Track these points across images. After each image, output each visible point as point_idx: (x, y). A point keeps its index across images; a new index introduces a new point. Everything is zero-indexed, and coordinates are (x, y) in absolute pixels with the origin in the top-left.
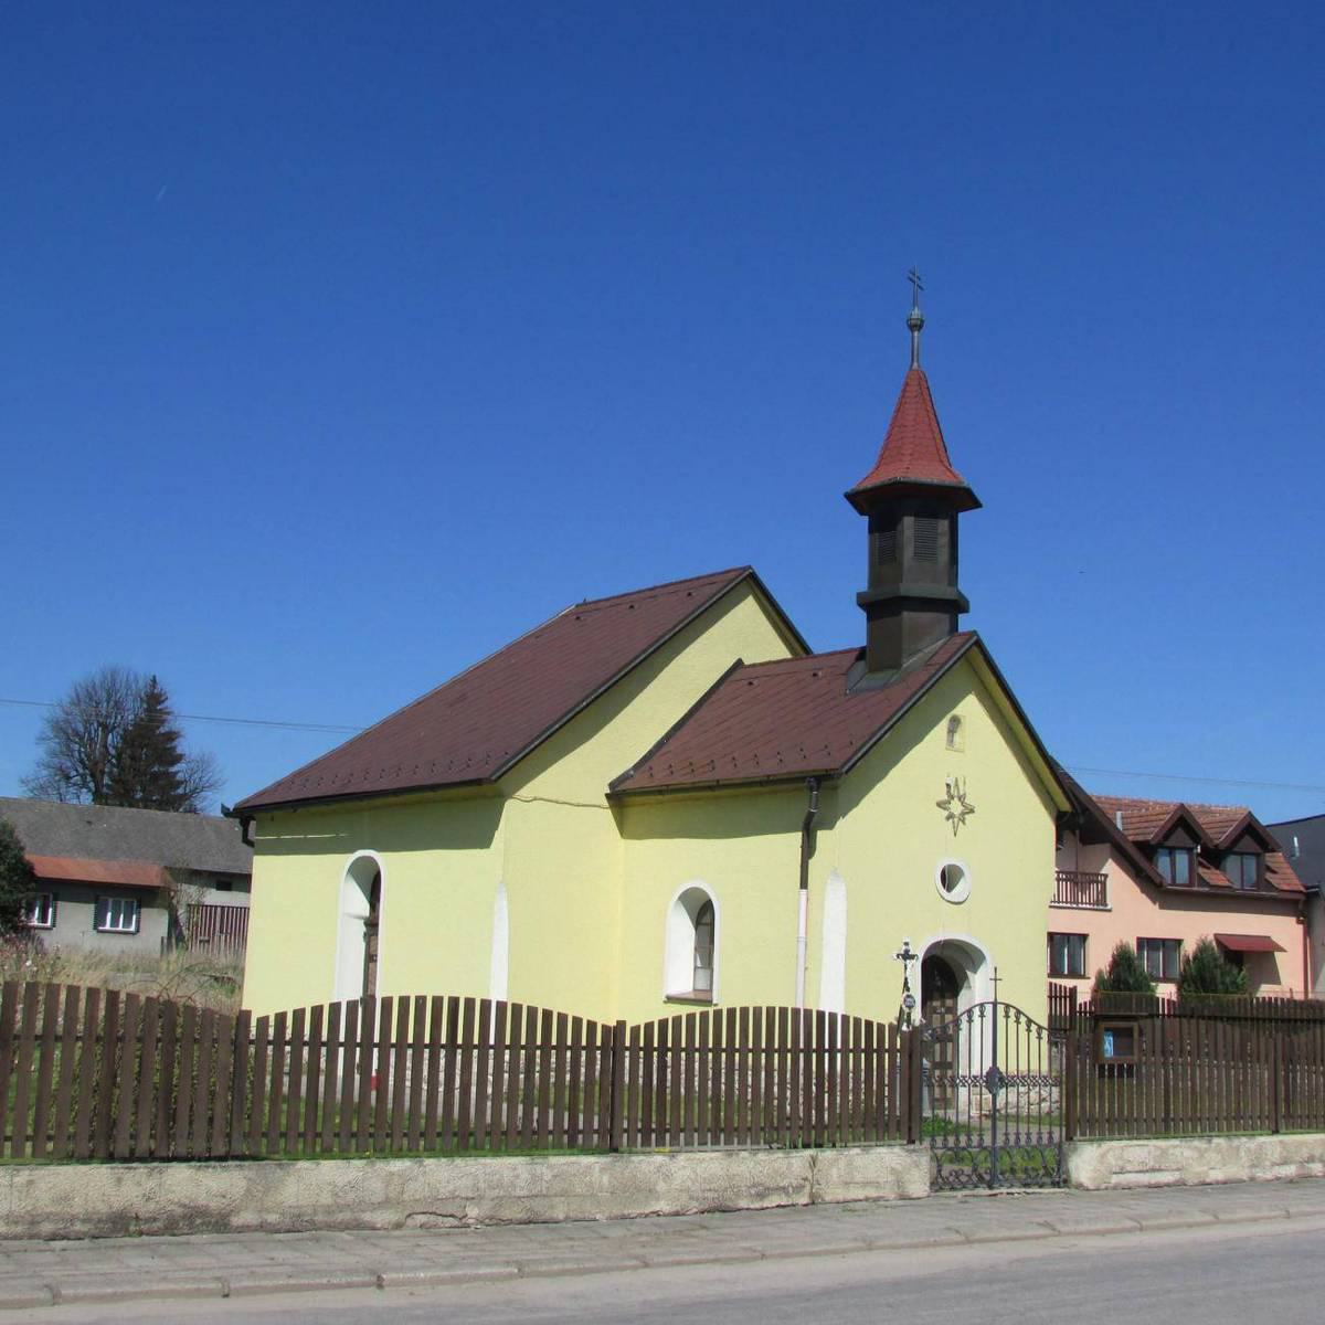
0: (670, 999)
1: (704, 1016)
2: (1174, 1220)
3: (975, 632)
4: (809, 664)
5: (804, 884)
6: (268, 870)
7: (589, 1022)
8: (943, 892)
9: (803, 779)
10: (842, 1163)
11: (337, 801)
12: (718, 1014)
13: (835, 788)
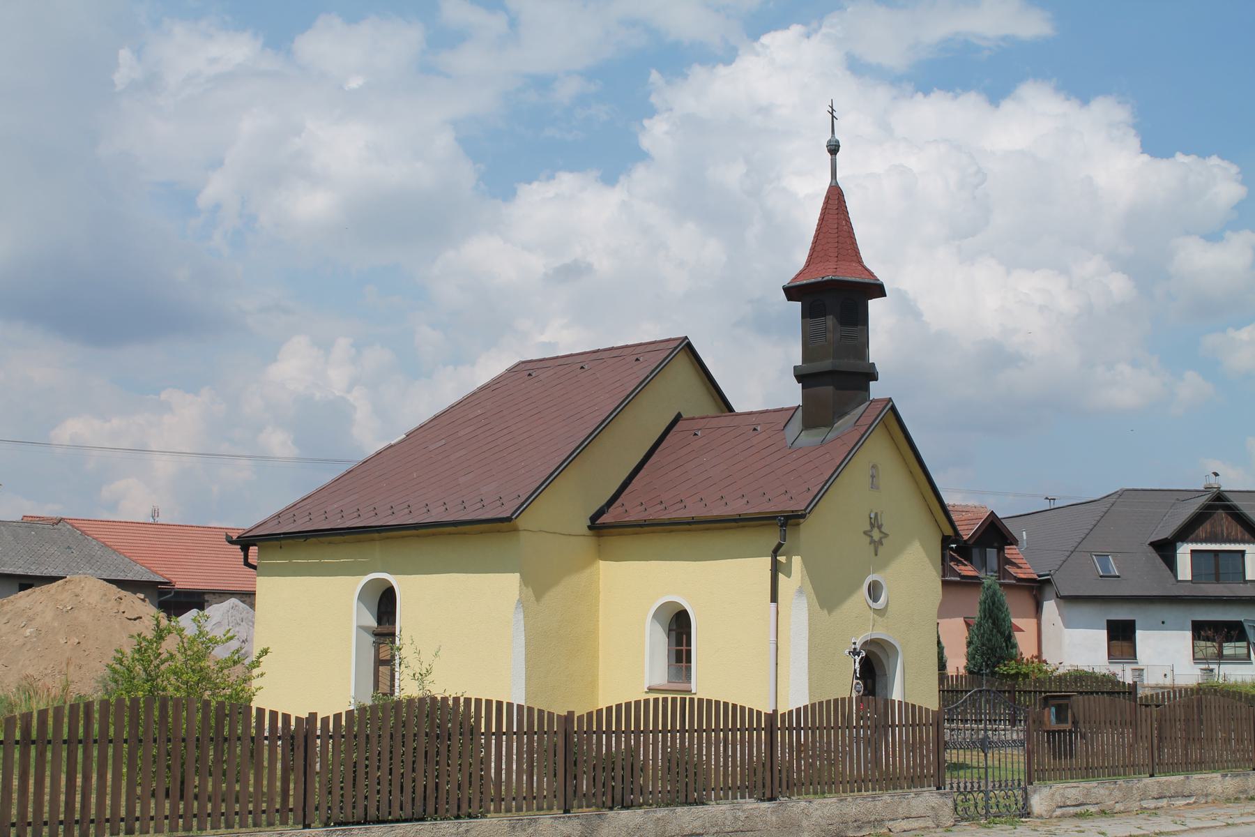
0: (651, 690)
1: (683, 700)
2: (1211, 824)
3: (890, 399)
4: (726, 420)
5: (774, 598)
6: (266, 587)
7: (284, 715)
8: (870, 602)
9: (775, 518)
10: (904, 805)
11: (341, 534)
12: (692, 700)
13: (798, 524)
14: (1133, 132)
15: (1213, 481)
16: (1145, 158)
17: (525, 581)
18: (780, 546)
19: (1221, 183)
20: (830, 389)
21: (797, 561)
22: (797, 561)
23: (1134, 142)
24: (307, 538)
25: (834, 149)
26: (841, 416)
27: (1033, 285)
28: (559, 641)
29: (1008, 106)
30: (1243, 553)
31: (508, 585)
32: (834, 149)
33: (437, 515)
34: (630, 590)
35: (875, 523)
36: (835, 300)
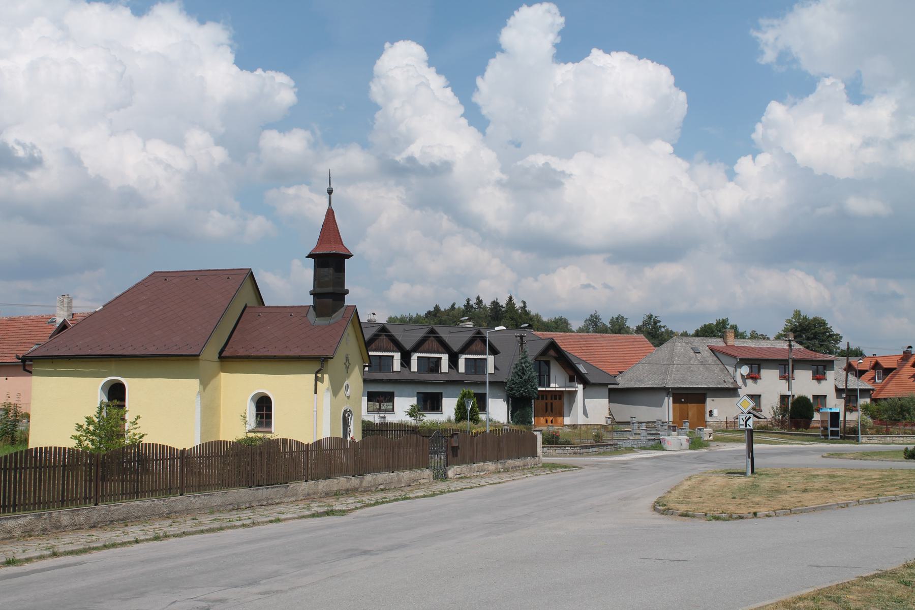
5: (316, 393)
14: (229, 50)
15: (372, 317)
16: (235, 69)
17: (201, 383)
18: (320, 370)
19: (281, 89)
20: (331, 300)
21: (326, 377)
22: (326, 377)
23: (231, 57)
24: (70, 359)
25: (330, 192)
26: (335, 312)
27: (160, 150)
28: (210, 412)
29: (145, 20)
30: (393, 357)
31: (195, 383)
32: (330, 192)
33: (152, 351)
34: (239, 388)
35: (347, 359)
36: (330, 262)
